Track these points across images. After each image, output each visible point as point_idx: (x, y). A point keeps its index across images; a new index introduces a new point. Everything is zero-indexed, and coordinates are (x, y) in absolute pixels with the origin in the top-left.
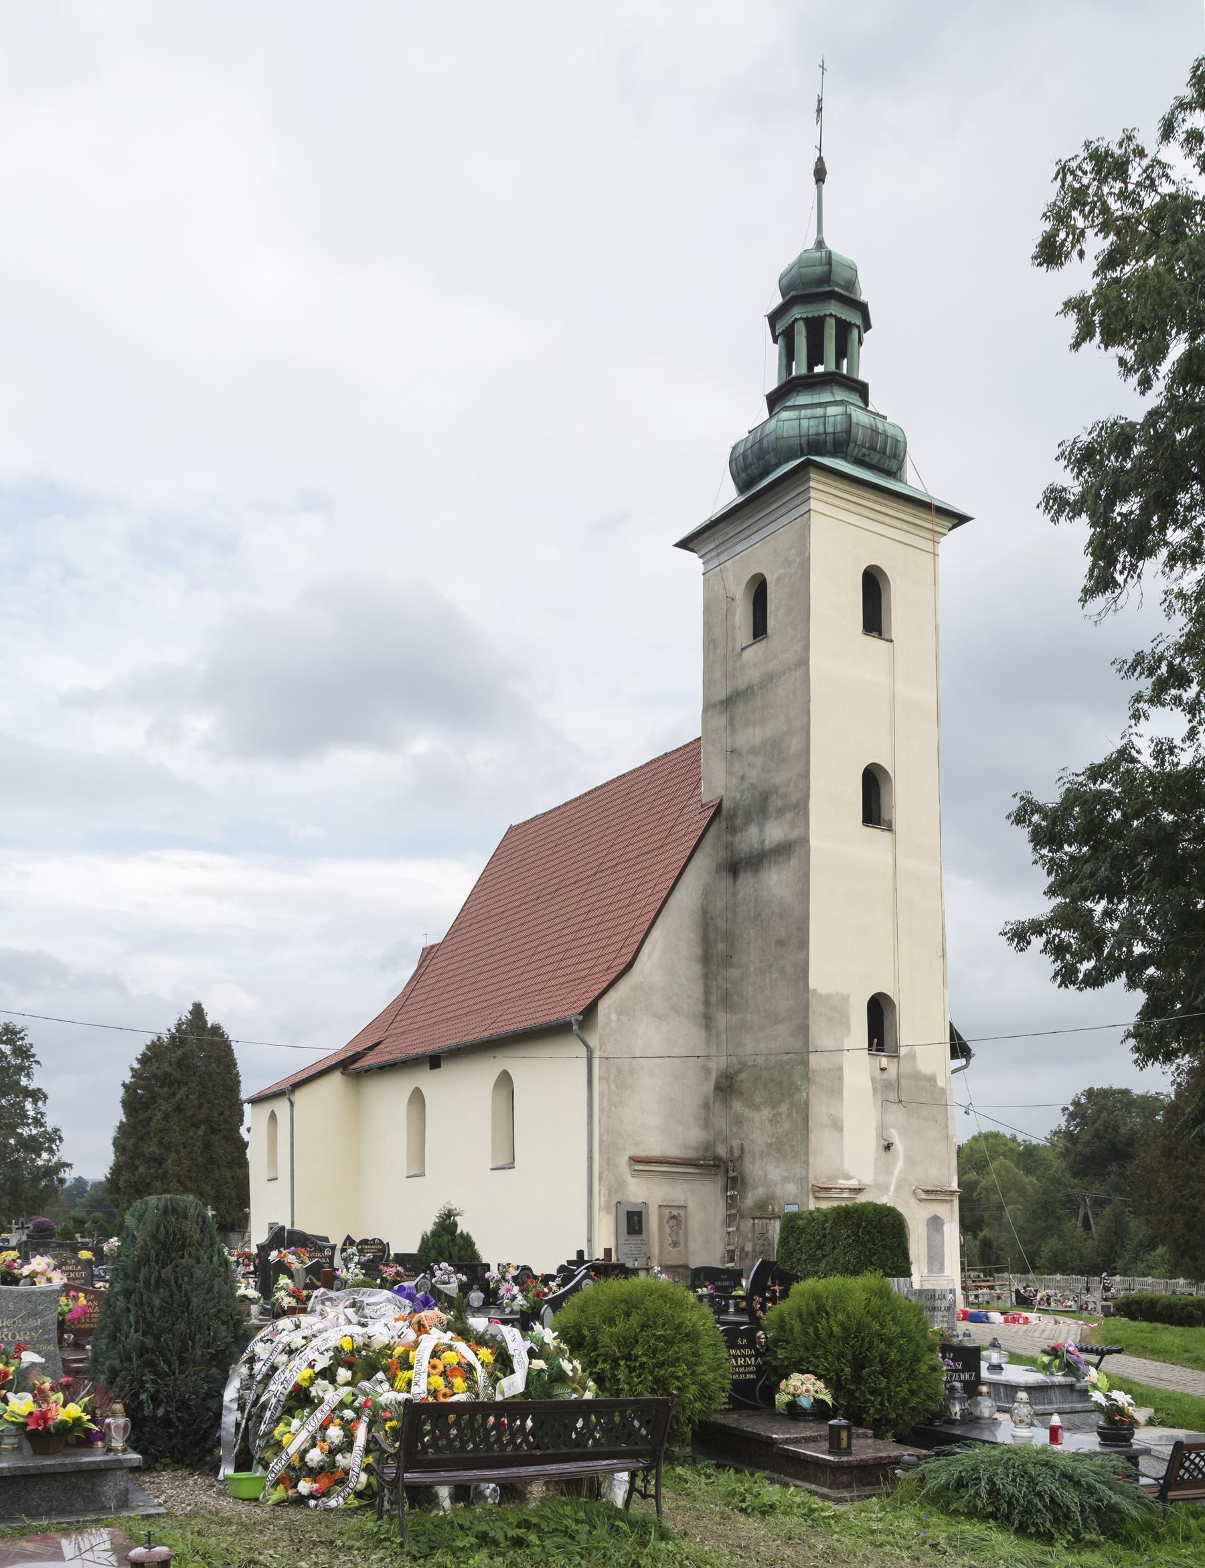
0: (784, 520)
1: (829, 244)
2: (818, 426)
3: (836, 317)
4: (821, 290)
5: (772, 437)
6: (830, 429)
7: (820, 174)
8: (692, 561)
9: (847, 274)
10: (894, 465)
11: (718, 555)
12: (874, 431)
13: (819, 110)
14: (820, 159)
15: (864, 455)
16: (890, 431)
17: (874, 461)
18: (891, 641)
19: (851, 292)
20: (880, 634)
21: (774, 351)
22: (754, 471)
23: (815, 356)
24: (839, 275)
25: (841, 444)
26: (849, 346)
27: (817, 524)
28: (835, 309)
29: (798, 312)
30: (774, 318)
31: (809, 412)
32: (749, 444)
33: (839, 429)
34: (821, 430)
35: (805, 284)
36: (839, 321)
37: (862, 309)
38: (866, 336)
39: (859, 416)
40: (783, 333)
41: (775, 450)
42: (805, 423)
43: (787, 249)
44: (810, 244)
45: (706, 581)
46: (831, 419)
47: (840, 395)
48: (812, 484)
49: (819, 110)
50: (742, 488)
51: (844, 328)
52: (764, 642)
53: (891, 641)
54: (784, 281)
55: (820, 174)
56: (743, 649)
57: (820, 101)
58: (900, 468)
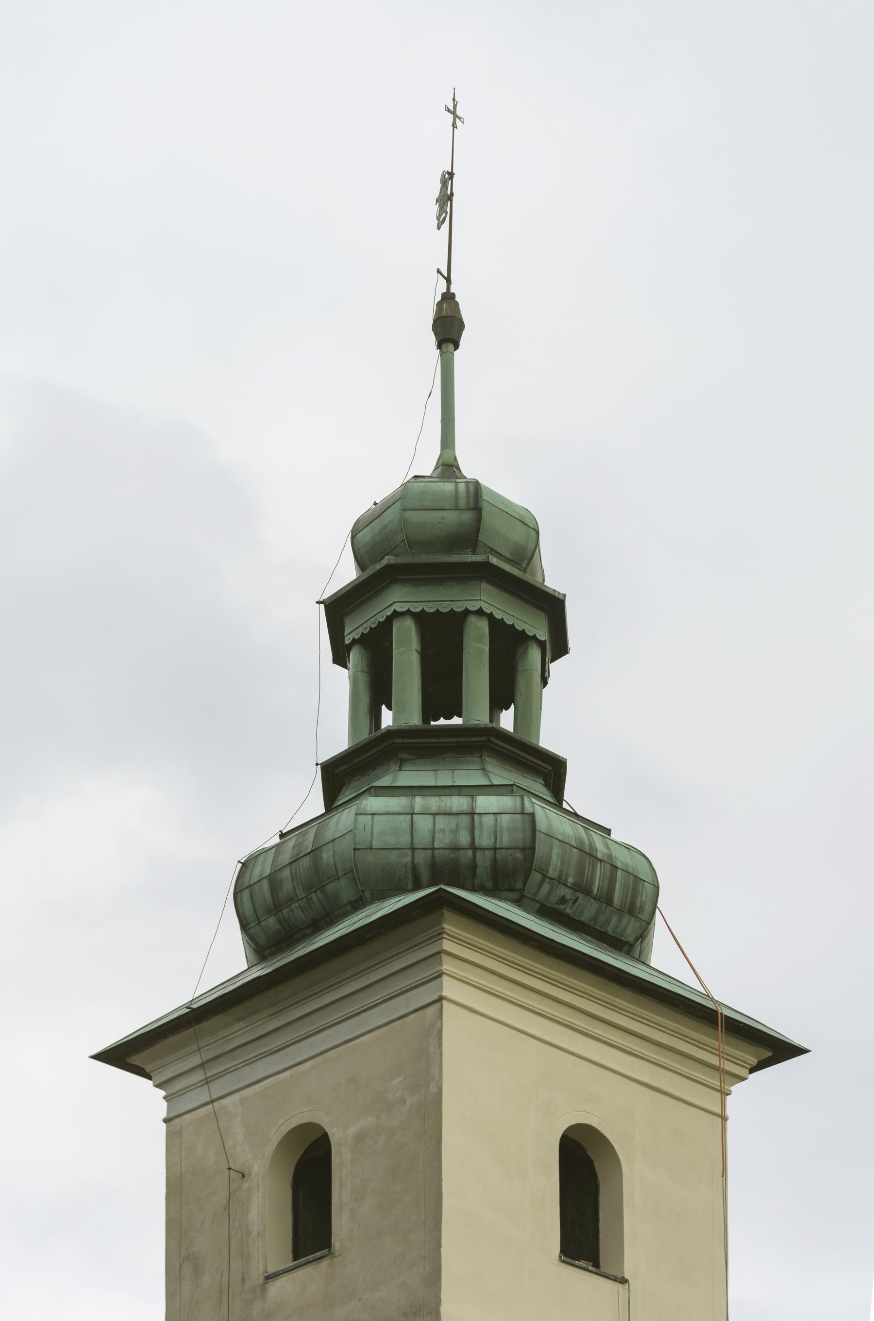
0: (375, 1017)
1: (469, 469)
2: (456, 831)
3: (490, 617)
4: (455, 558)
5: (345, 846)
6: (484, 840)
7: (448, 328)
8: (141, 1099)
9: (517, 535)
10: (629, 929)
11: (207, 1081)
12: (588, 854)
13: (446, 199)
14: (448, 297)
15: (563, 900)
16: (622, 858)
17: (585, 918)
18: (623, 1281)
19: (525, 570)
20: (597, 1265)
21: (339, 684)
22: (297, 913)
23: (442, 692)
24: (498, 533)
25: (514, 869)
26: (521, 682)
27: (455, 1026)
28: (487, 599)
29: (398, 599)
30: (338, 608)
31: (434, 803)
32: (286, 857)
33: (505, 840)
34: (464, 839)
35: (412, 544)
36: (497, 627)
37: (553, 607)
38: (556, 668)
39: (547, 818)
40: (363, 641)
41: (352, 873)
42: (424, 824)
43: (389, 462)
44: (427, 466)
45: (172, 1139)
46: (488, 821)
47: (500, 775)
48: (447, 945)
49: (446, 199)
50: (260, 946)
51: (507, 646)
52: (325, 1263)
53: (623, 1281)
54: (366, 535)
55: (448, 328)
56: (270, 1277)
57: (448, 177)
58: (644, 933)
